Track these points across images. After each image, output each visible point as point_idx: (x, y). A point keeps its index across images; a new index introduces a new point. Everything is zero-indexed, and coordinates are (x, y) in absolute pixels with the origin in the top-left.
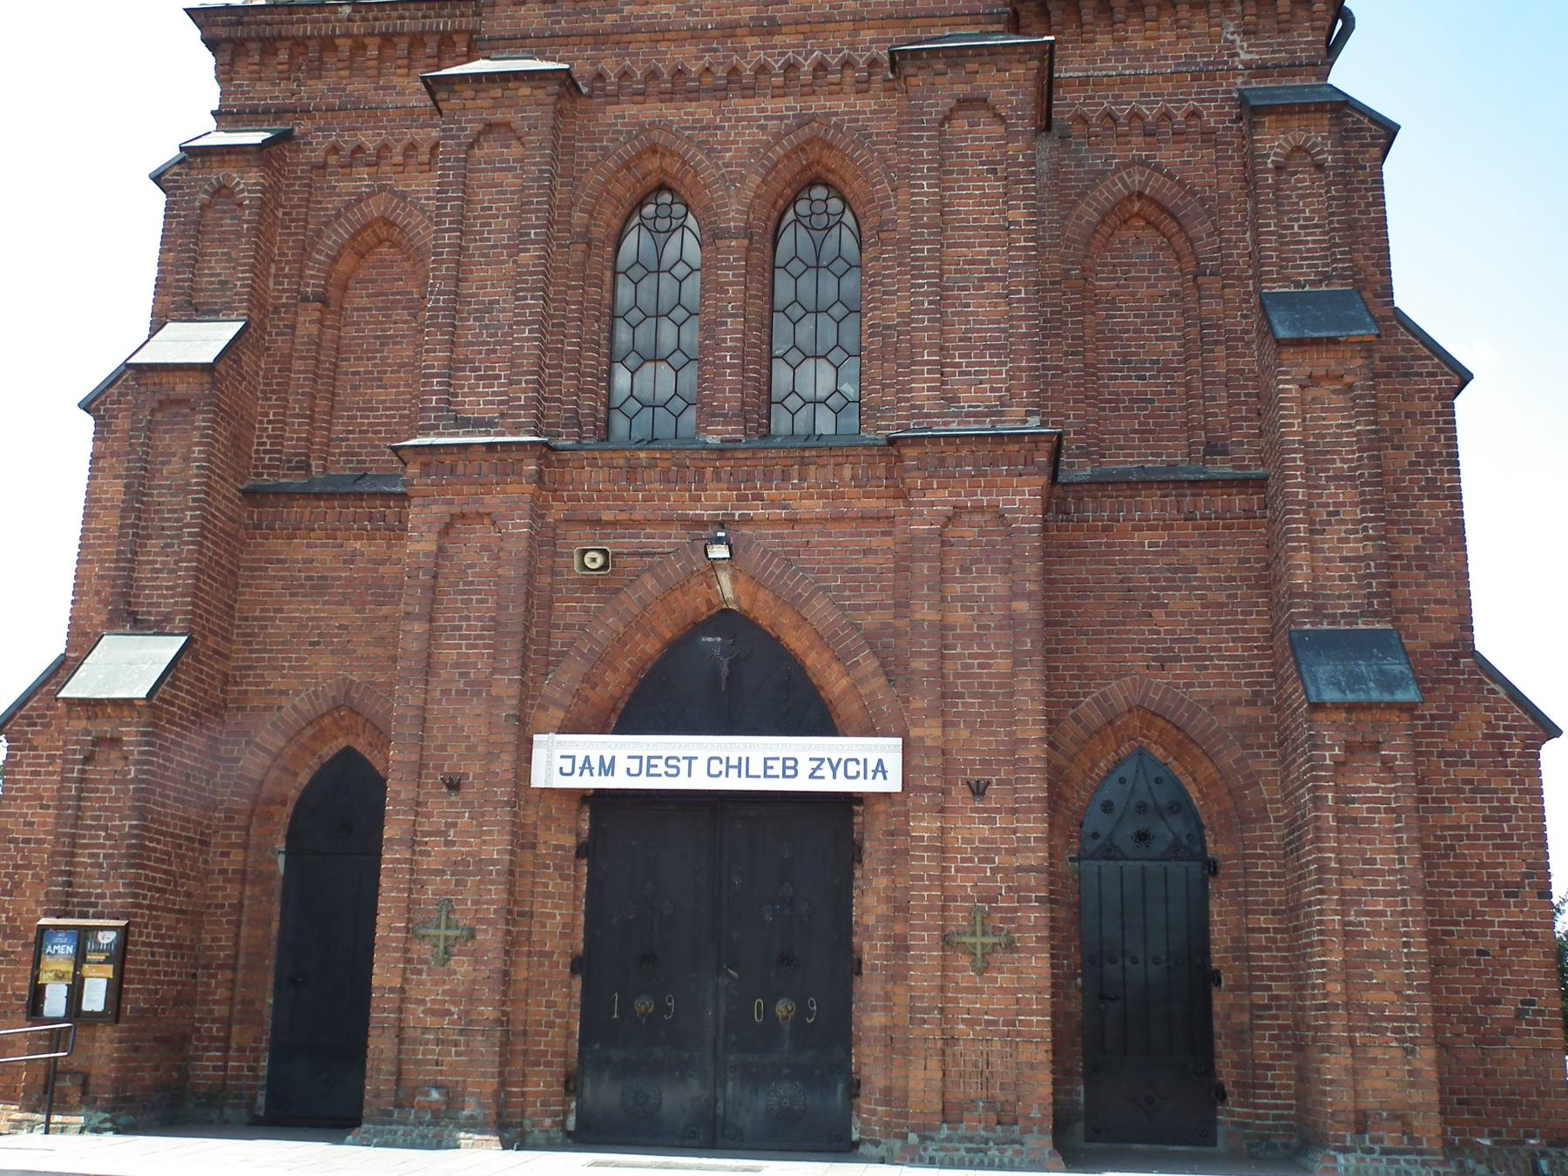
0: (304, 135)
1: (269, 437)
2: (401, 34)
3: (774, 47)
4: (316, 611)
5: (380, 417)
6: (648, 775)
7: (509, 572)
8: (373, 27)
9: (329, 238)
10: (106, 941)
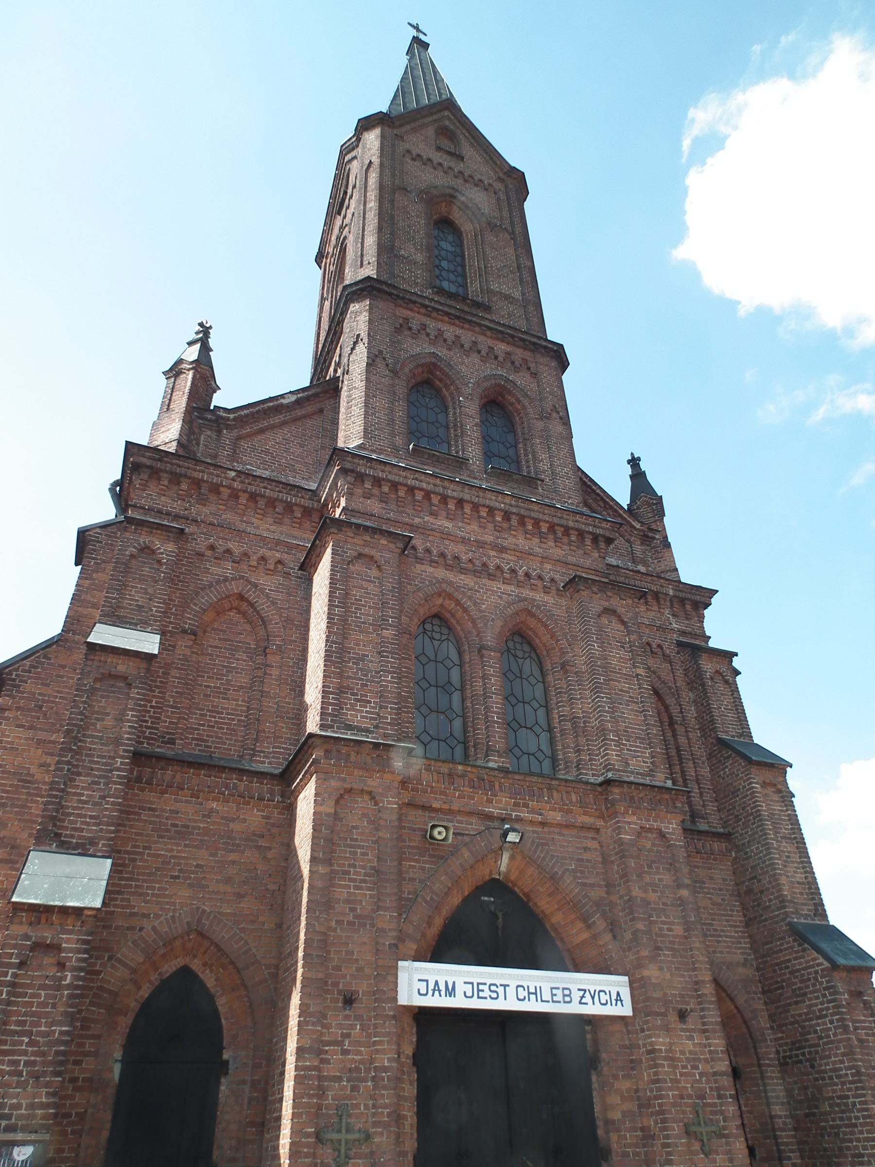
0: (192, 534)
1: (150, 717)
2: (263, 496)
3: (504, 559)
4: (178, 851)
5: (224, 718)
6: (479, 997)
7: (385, 834)
8: (247, 488)
9: (203, 598)
10: (22, 1158)
